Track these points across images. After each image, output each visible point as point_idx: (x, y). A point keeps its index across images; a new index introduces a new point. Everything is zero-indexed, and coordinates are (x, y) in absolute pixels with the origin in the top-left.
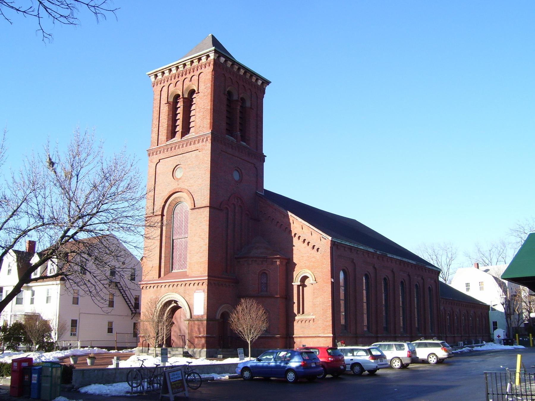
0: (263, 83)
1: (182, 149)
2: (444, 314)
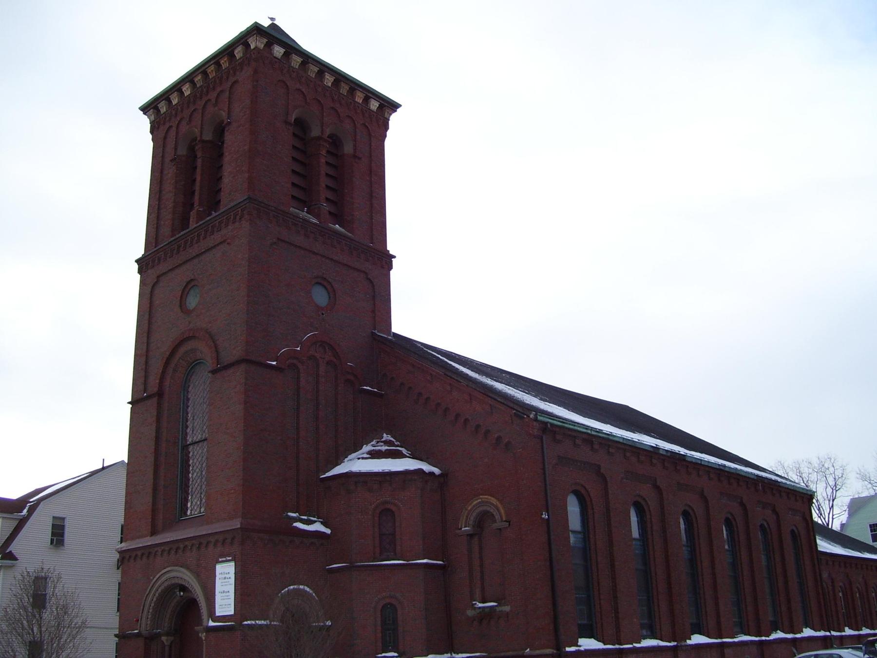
0: (381, 107)
1: (196, 245)
2: (830, 588)
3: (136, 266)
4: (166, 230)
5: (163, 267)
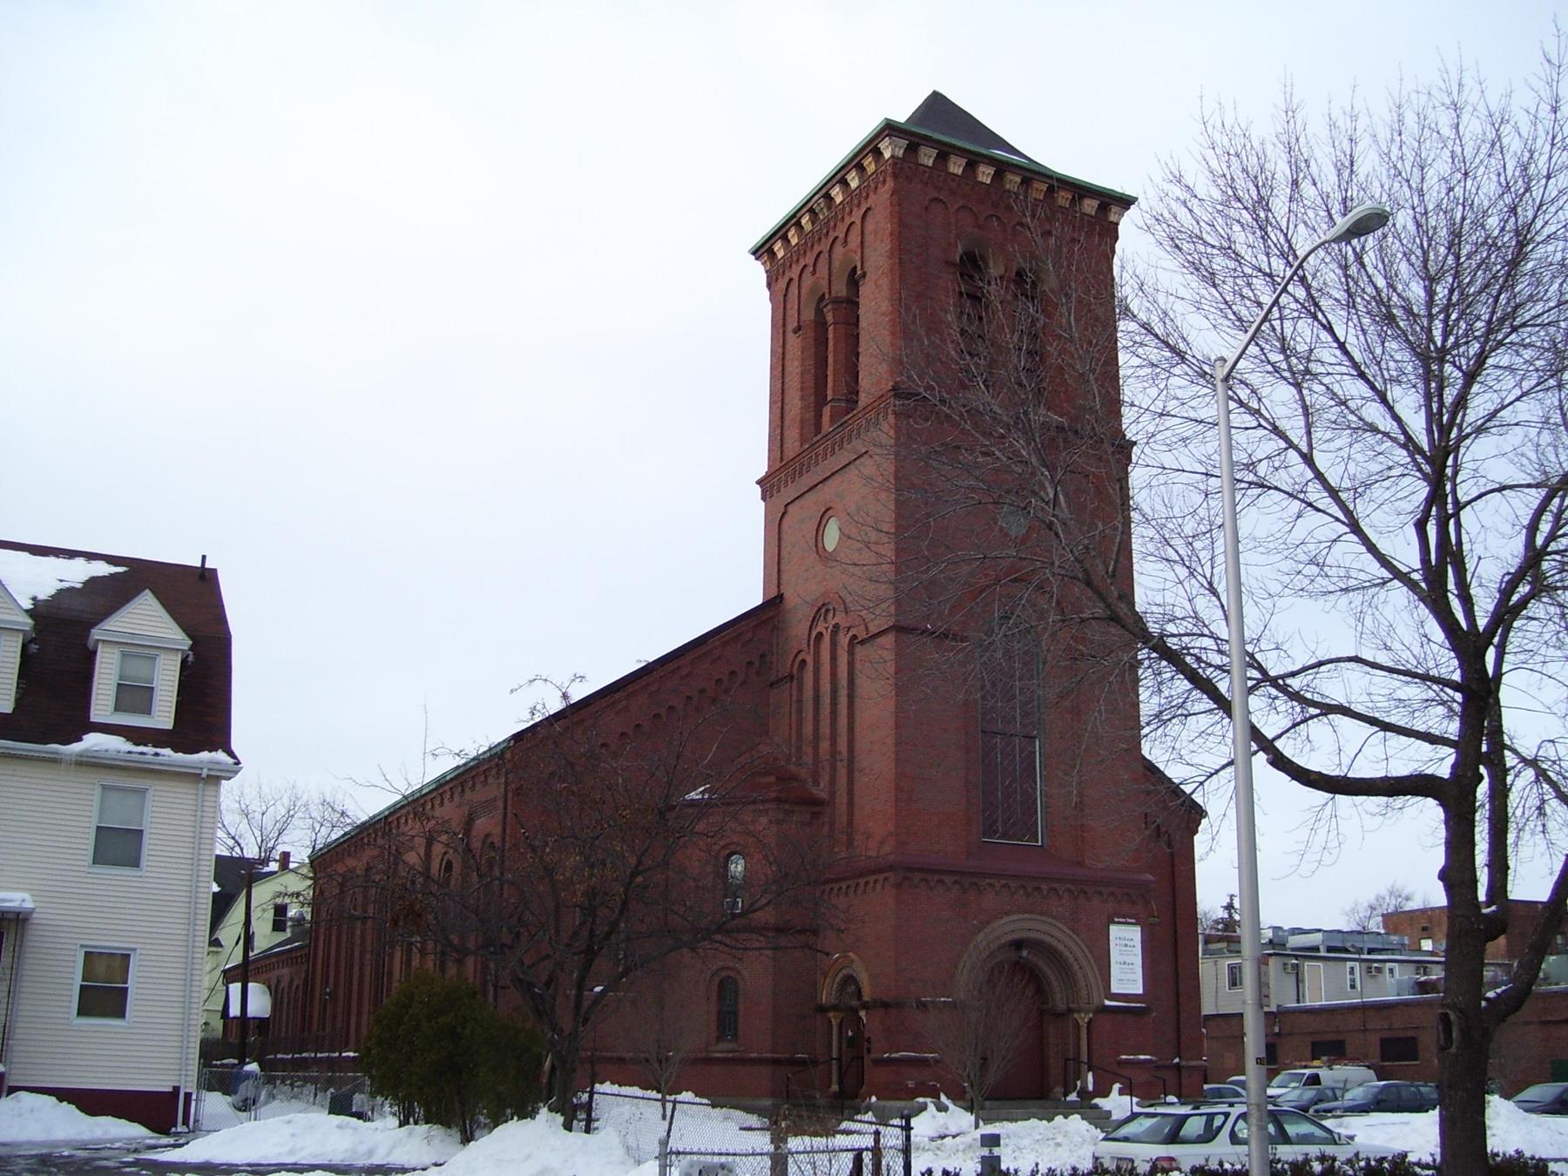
3: (758, 489)
4: (792, 435)
5: (789, 492)
